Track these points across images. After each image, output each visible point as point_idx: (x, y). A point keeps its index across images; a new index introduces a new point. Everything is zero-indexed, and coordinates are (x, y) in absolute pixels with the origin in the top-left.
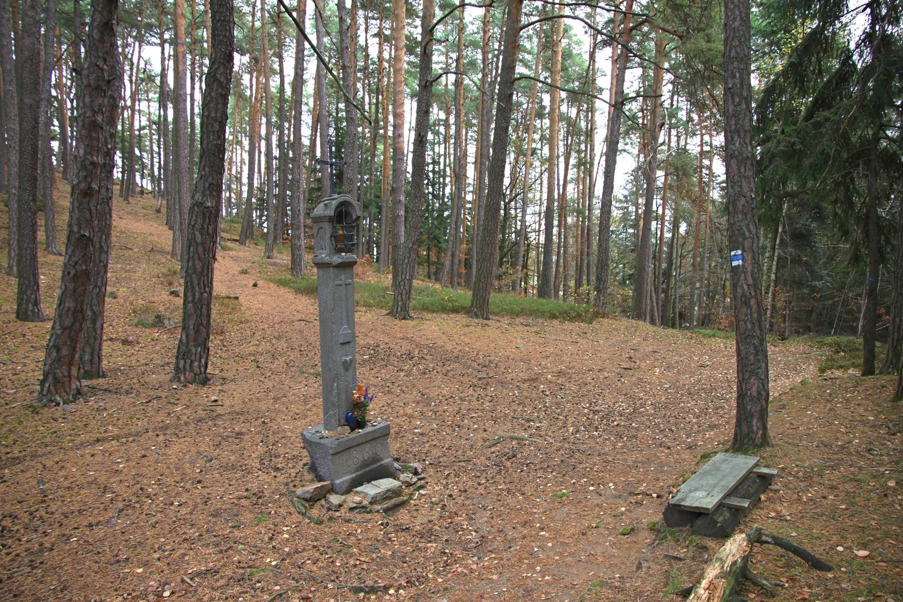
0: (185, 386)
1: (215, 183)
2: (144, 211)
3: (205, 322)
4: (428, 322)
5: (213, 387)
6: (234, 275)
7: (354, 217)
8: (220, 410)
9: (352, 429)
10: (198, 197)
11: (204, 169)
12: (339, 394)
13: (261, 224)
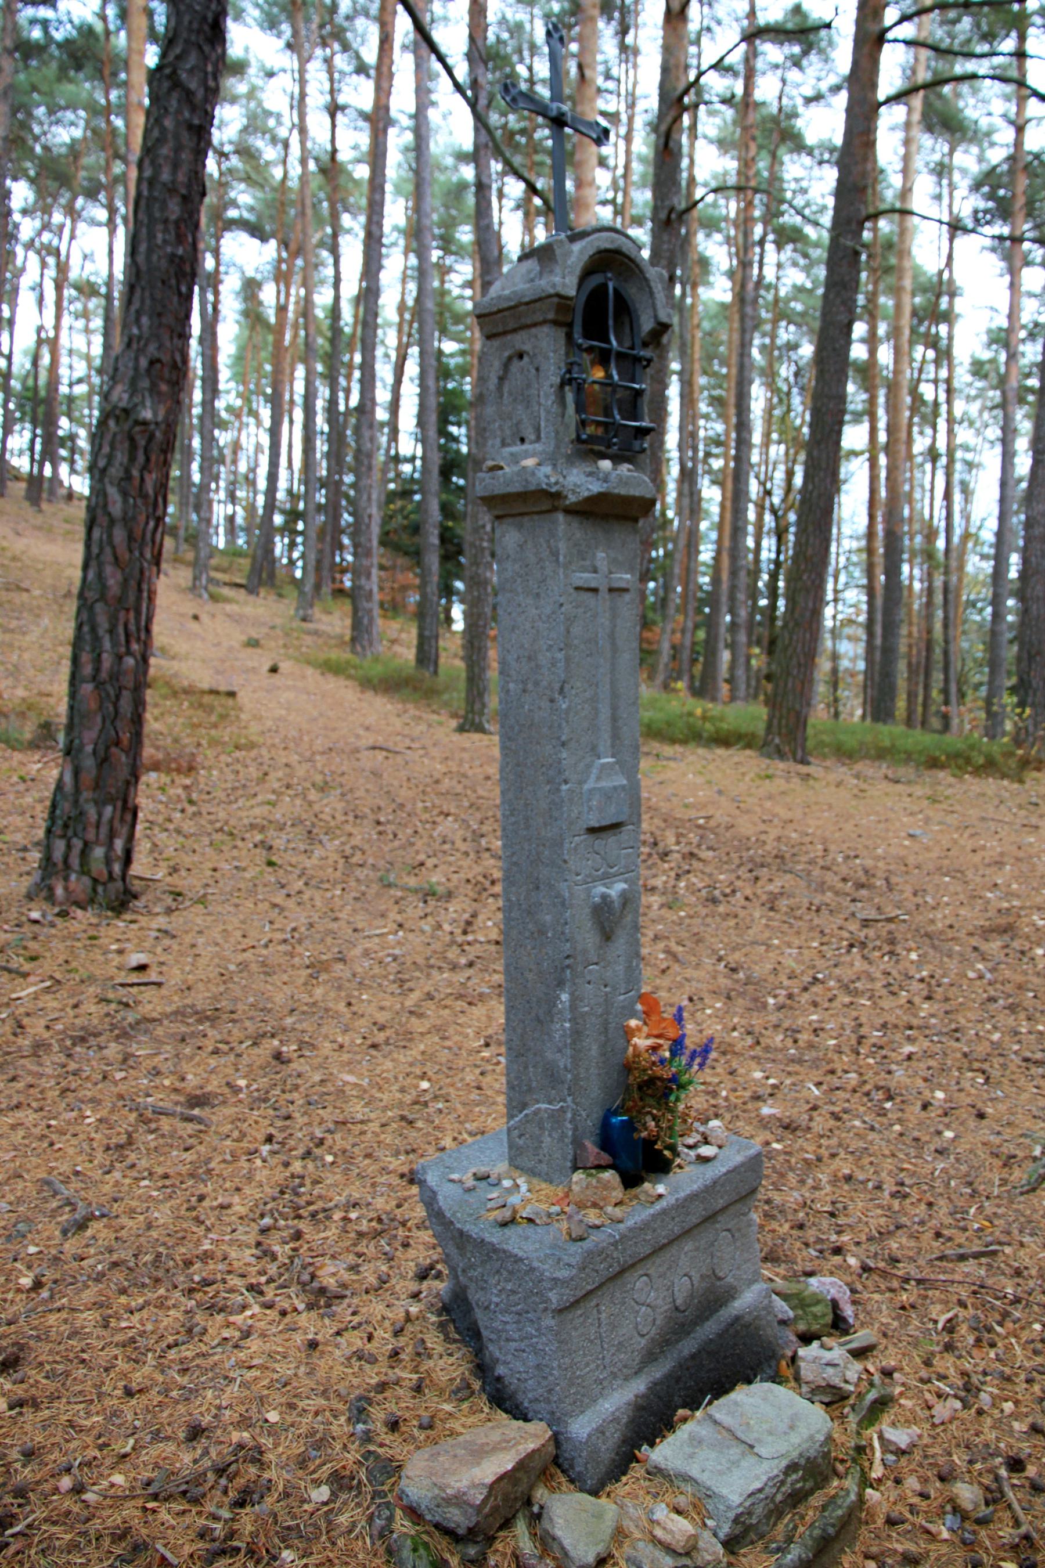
0: (63, 914)
1: (166, 358)
2: (68, 526)
3: (126, 737)
4: (672, 764)
5: (144, 921)
6: (231, 649)
7: (647, 325)
8: (151, 1003)
9: (631, 1181)
10: (121, 395)
11: (137, 321)
12: (577, 1034)
13: (292, 563)
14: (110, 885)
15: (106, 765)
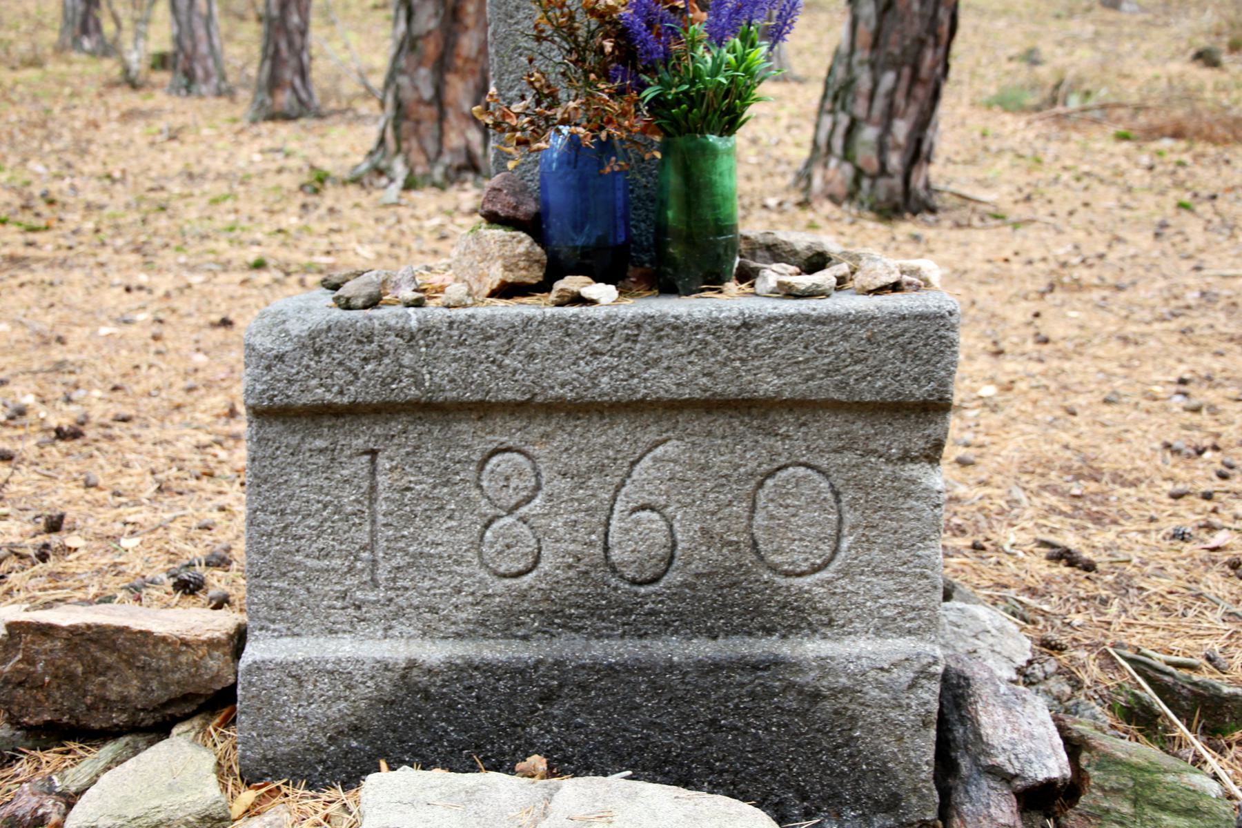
14: (882, 183)
15: (889, 15)
